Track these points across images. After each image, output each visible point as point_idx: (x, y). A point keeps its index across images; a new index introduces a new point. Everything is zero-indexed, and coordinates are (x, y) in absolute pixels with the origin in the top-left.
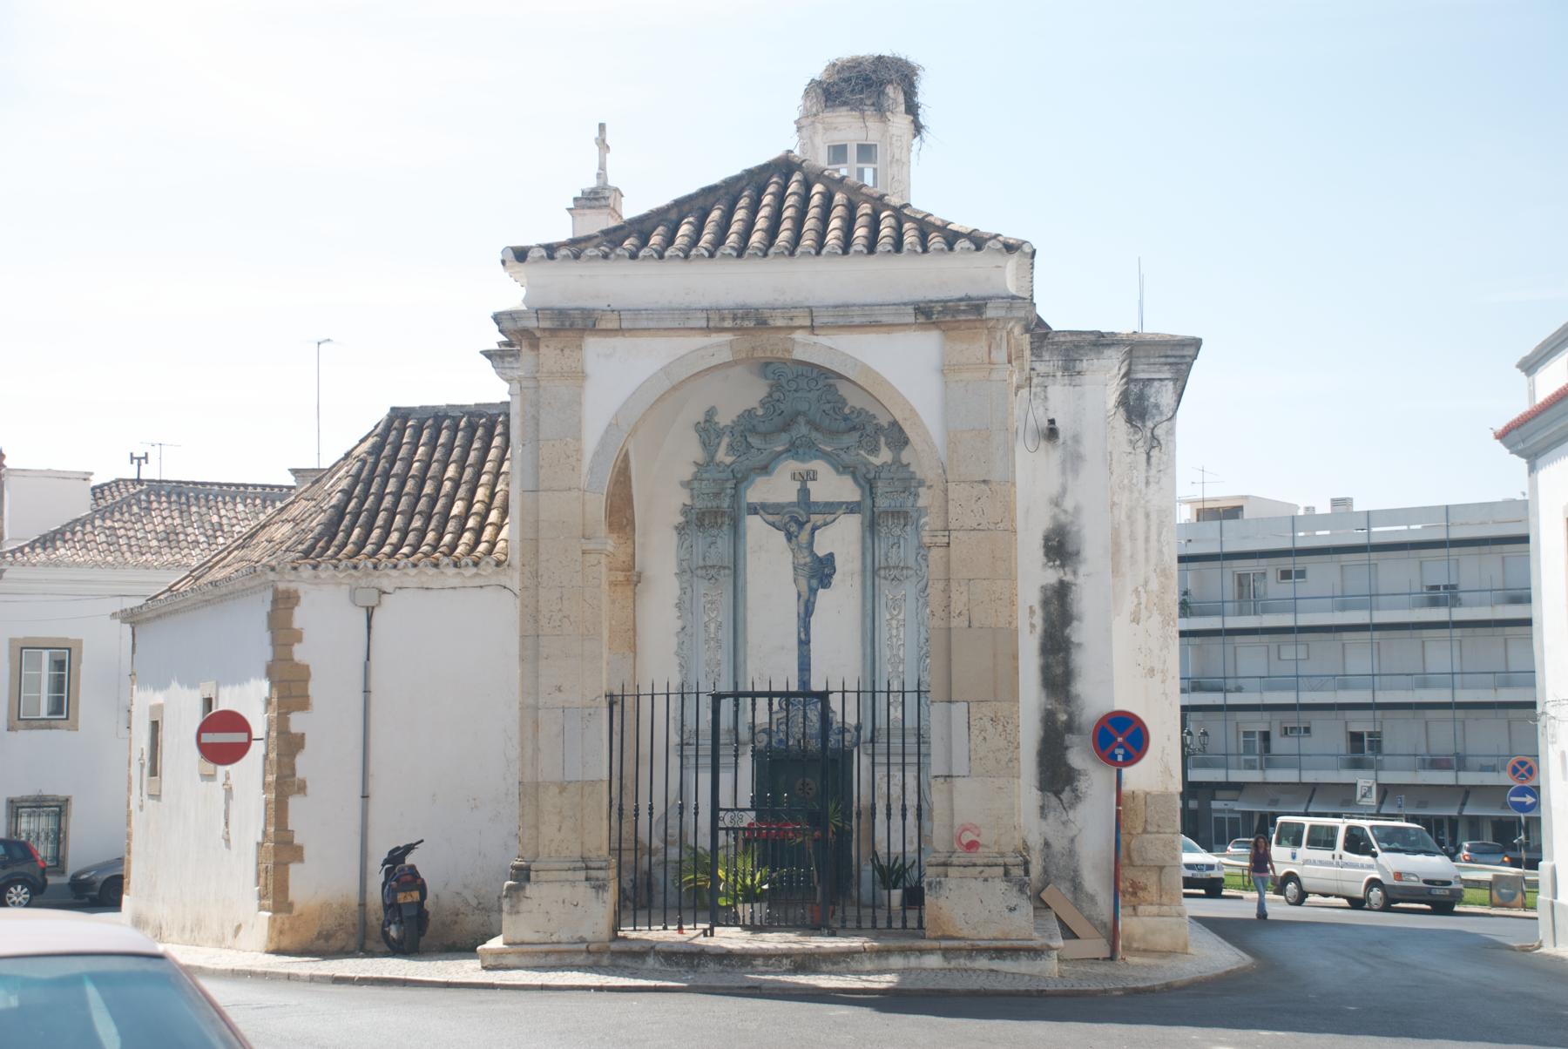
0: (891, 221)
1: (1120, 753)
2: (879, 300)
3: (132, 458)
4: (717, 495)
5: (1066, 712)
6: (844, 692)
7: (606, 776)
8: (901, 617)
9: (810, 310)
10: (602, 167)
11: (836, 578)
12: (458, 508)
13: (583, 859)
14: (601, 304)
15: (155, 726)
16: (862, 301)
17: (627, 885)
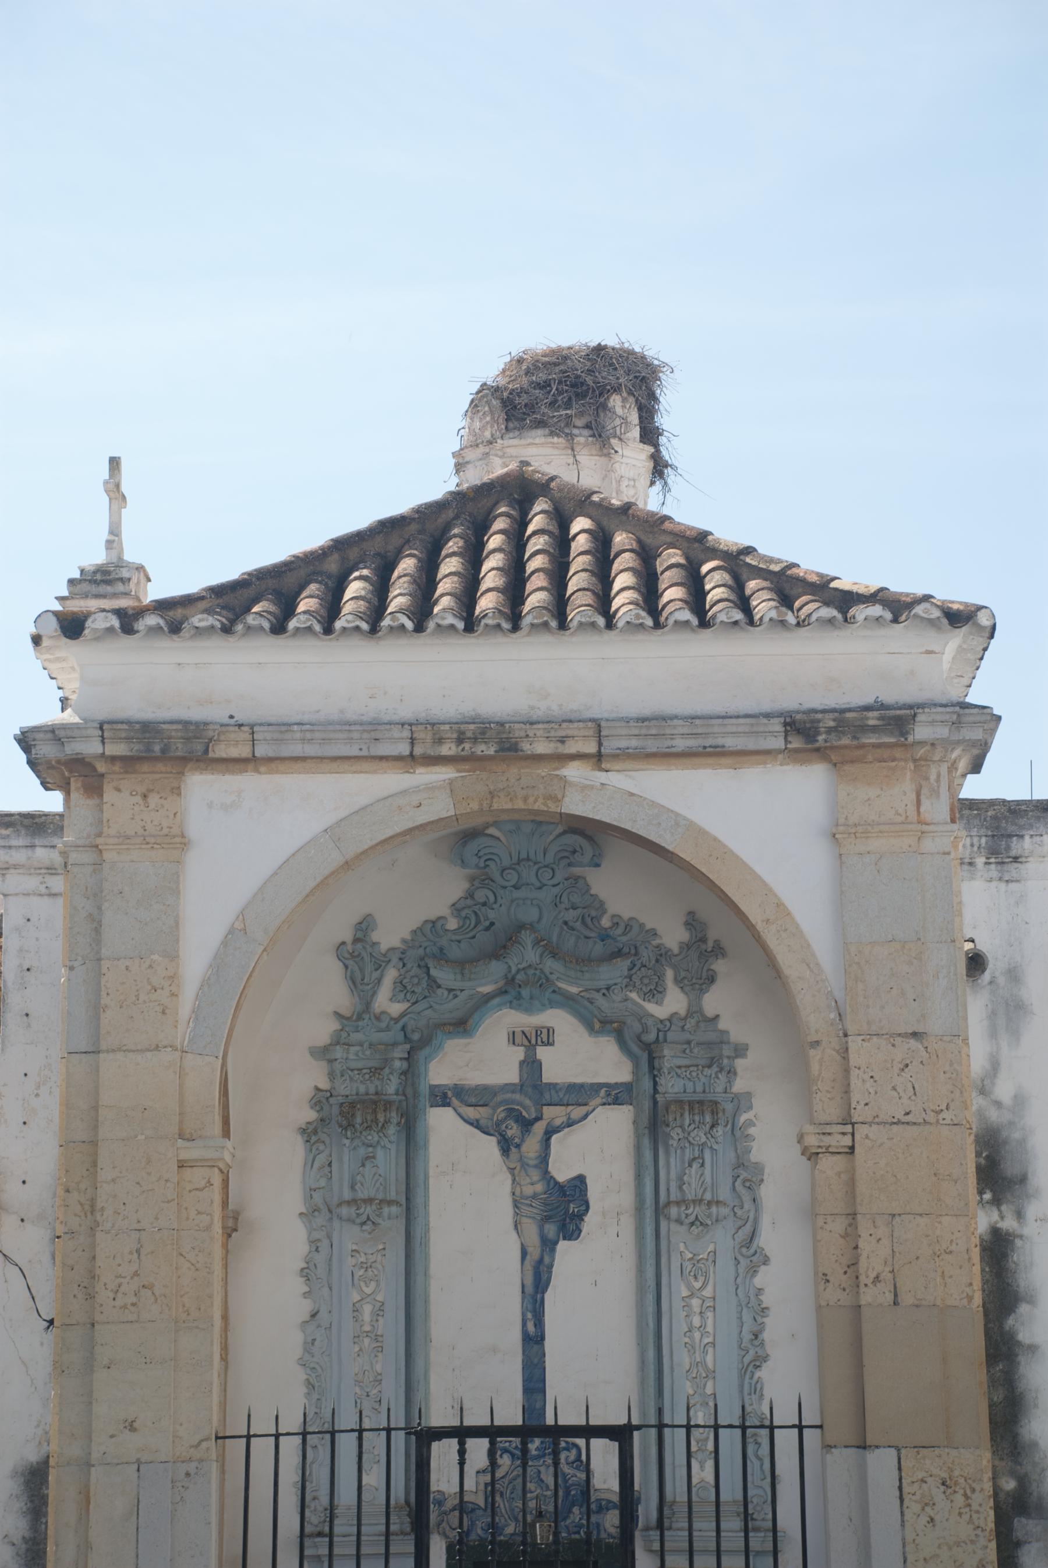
2: (719, 710)
4: (375, 1071)
5: (1013, 1474)
8: (708, 1292)
9: (598, 725)
10: (115, 531)
11: (590, 1222)
14: (217, 714)
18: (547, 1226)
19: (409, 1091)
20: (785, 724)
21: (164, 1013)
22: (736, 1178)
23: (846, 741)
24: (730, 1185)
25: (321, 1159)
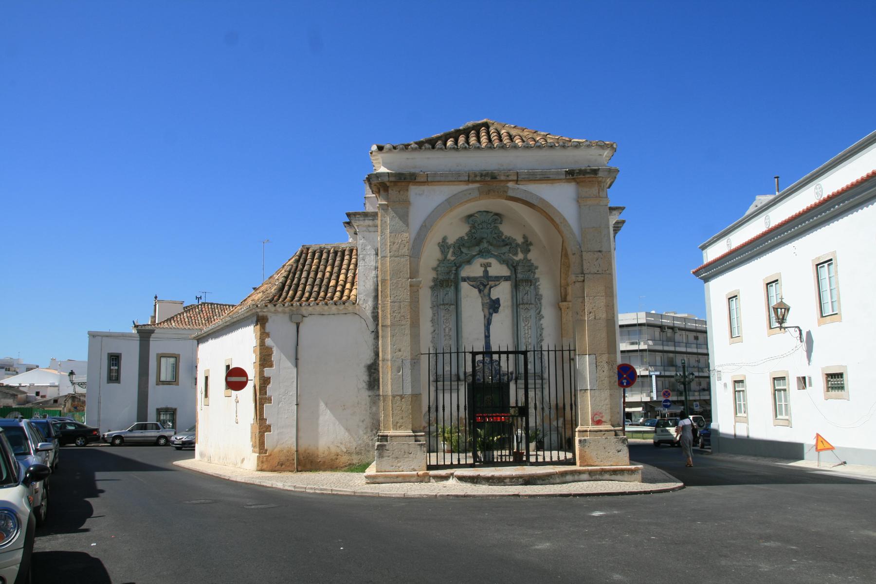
1: (625, 381)
4: (448, 273)
12: (333, 283)
15: (207, 378)
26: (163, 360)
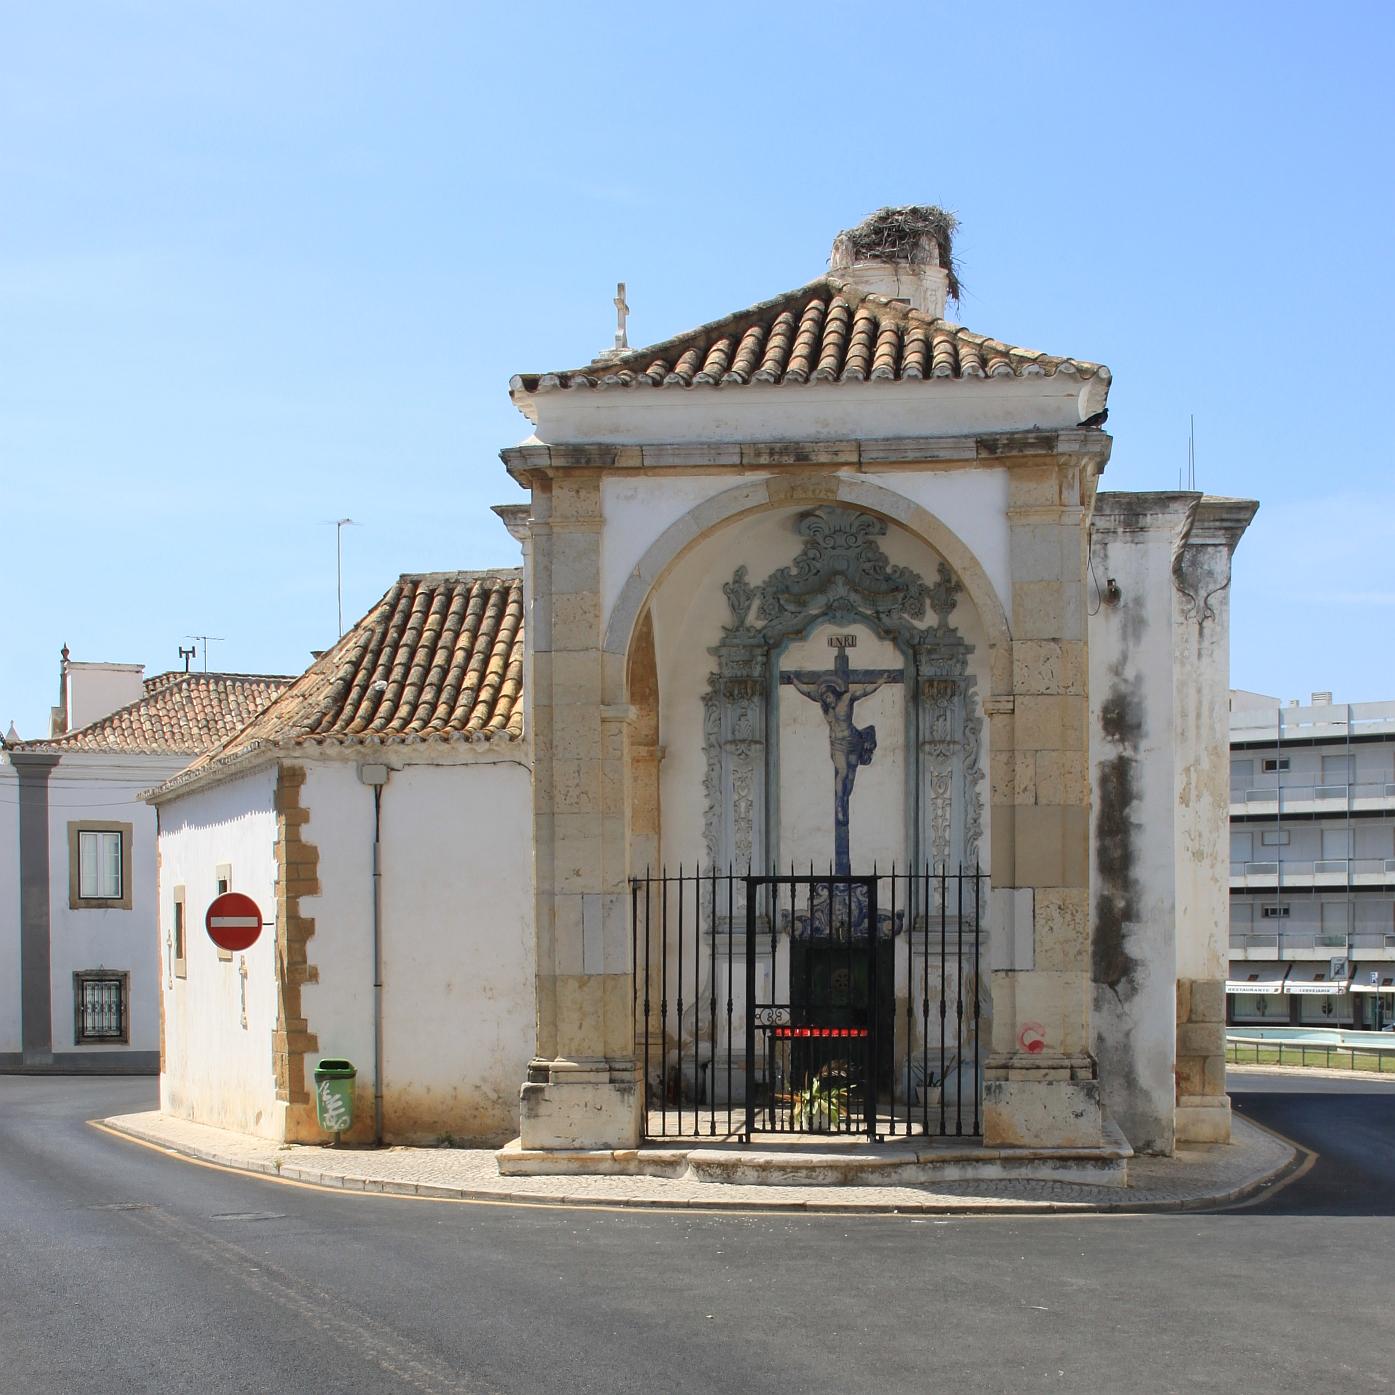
0: (947, 347)
2: (937, 433)
3: (181, 652)
4: (748, 662)
6: (894, 877)
7: (630, 970)
8: (947, 795)
11: (877, 753)
12: (471, 679)
13: (607, 1060)
15: (179, 906)
16: (916, 433)
17: (654, 1081)
18: (851, 757)
19: (767, 675)
20: (977, 442)
21: (591, 627)
22: (966, 727)
23: (1015, 453)
24: (961, 731)
25: (715, 716)
26: (87, 840)
